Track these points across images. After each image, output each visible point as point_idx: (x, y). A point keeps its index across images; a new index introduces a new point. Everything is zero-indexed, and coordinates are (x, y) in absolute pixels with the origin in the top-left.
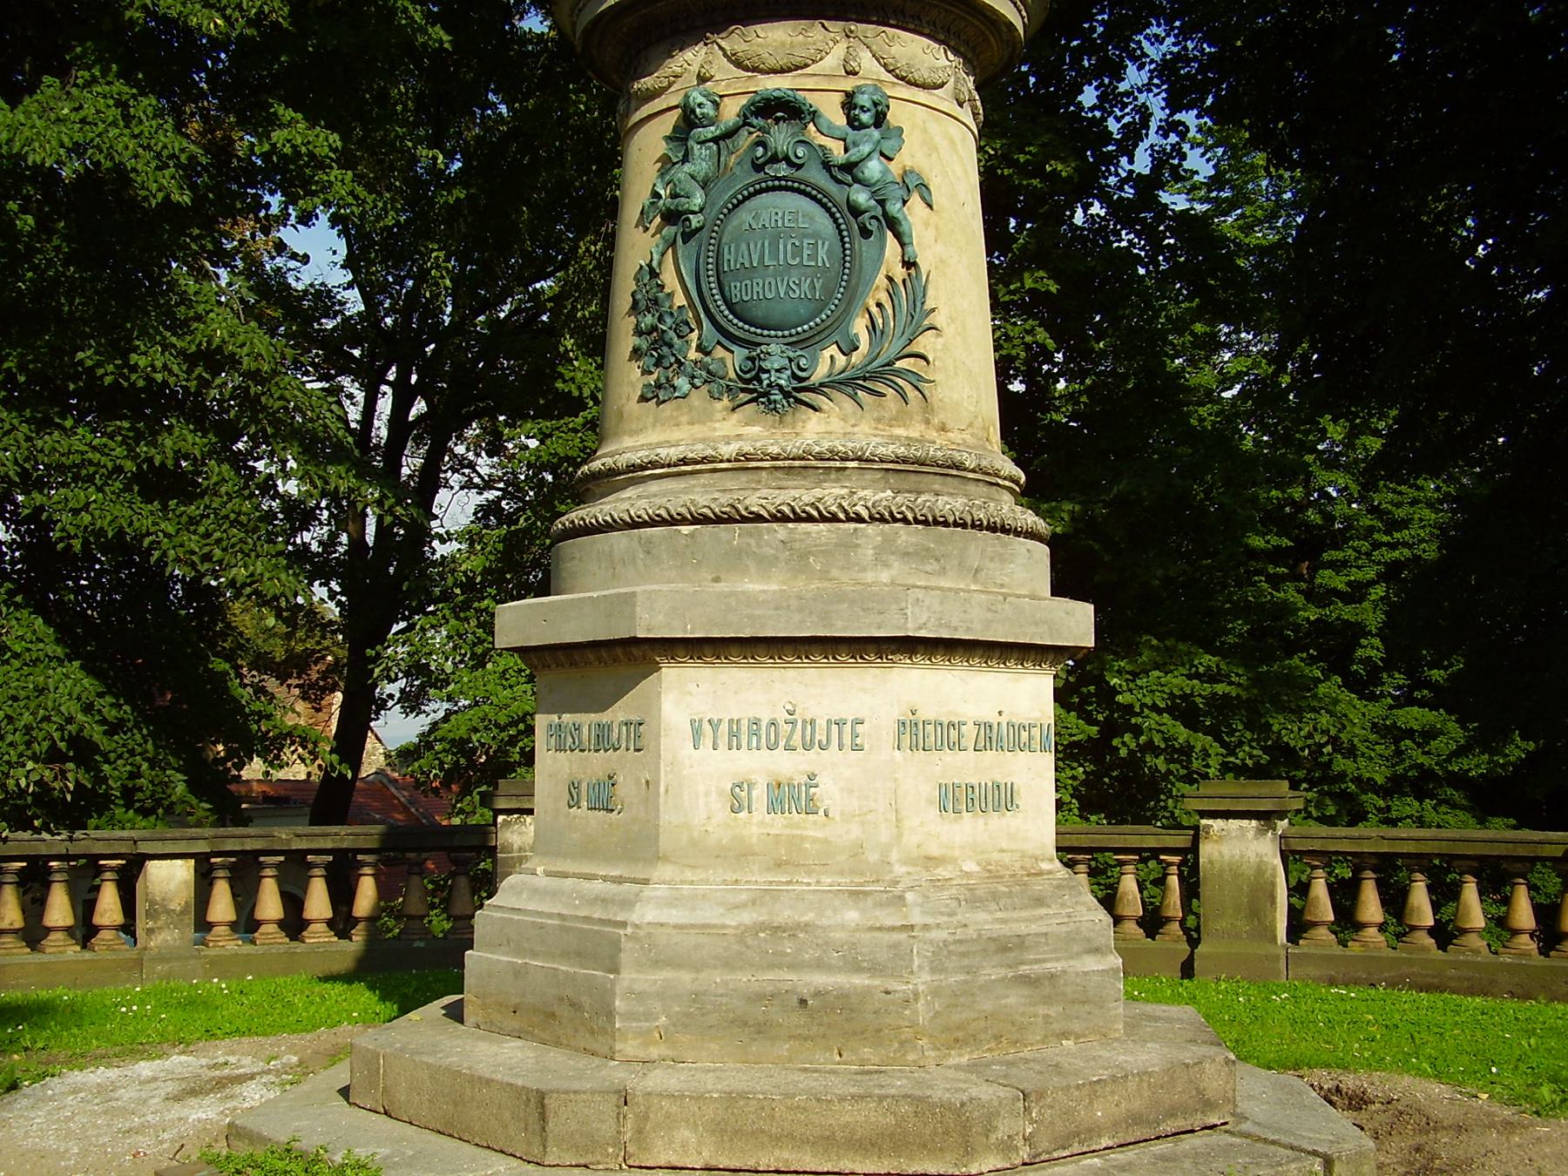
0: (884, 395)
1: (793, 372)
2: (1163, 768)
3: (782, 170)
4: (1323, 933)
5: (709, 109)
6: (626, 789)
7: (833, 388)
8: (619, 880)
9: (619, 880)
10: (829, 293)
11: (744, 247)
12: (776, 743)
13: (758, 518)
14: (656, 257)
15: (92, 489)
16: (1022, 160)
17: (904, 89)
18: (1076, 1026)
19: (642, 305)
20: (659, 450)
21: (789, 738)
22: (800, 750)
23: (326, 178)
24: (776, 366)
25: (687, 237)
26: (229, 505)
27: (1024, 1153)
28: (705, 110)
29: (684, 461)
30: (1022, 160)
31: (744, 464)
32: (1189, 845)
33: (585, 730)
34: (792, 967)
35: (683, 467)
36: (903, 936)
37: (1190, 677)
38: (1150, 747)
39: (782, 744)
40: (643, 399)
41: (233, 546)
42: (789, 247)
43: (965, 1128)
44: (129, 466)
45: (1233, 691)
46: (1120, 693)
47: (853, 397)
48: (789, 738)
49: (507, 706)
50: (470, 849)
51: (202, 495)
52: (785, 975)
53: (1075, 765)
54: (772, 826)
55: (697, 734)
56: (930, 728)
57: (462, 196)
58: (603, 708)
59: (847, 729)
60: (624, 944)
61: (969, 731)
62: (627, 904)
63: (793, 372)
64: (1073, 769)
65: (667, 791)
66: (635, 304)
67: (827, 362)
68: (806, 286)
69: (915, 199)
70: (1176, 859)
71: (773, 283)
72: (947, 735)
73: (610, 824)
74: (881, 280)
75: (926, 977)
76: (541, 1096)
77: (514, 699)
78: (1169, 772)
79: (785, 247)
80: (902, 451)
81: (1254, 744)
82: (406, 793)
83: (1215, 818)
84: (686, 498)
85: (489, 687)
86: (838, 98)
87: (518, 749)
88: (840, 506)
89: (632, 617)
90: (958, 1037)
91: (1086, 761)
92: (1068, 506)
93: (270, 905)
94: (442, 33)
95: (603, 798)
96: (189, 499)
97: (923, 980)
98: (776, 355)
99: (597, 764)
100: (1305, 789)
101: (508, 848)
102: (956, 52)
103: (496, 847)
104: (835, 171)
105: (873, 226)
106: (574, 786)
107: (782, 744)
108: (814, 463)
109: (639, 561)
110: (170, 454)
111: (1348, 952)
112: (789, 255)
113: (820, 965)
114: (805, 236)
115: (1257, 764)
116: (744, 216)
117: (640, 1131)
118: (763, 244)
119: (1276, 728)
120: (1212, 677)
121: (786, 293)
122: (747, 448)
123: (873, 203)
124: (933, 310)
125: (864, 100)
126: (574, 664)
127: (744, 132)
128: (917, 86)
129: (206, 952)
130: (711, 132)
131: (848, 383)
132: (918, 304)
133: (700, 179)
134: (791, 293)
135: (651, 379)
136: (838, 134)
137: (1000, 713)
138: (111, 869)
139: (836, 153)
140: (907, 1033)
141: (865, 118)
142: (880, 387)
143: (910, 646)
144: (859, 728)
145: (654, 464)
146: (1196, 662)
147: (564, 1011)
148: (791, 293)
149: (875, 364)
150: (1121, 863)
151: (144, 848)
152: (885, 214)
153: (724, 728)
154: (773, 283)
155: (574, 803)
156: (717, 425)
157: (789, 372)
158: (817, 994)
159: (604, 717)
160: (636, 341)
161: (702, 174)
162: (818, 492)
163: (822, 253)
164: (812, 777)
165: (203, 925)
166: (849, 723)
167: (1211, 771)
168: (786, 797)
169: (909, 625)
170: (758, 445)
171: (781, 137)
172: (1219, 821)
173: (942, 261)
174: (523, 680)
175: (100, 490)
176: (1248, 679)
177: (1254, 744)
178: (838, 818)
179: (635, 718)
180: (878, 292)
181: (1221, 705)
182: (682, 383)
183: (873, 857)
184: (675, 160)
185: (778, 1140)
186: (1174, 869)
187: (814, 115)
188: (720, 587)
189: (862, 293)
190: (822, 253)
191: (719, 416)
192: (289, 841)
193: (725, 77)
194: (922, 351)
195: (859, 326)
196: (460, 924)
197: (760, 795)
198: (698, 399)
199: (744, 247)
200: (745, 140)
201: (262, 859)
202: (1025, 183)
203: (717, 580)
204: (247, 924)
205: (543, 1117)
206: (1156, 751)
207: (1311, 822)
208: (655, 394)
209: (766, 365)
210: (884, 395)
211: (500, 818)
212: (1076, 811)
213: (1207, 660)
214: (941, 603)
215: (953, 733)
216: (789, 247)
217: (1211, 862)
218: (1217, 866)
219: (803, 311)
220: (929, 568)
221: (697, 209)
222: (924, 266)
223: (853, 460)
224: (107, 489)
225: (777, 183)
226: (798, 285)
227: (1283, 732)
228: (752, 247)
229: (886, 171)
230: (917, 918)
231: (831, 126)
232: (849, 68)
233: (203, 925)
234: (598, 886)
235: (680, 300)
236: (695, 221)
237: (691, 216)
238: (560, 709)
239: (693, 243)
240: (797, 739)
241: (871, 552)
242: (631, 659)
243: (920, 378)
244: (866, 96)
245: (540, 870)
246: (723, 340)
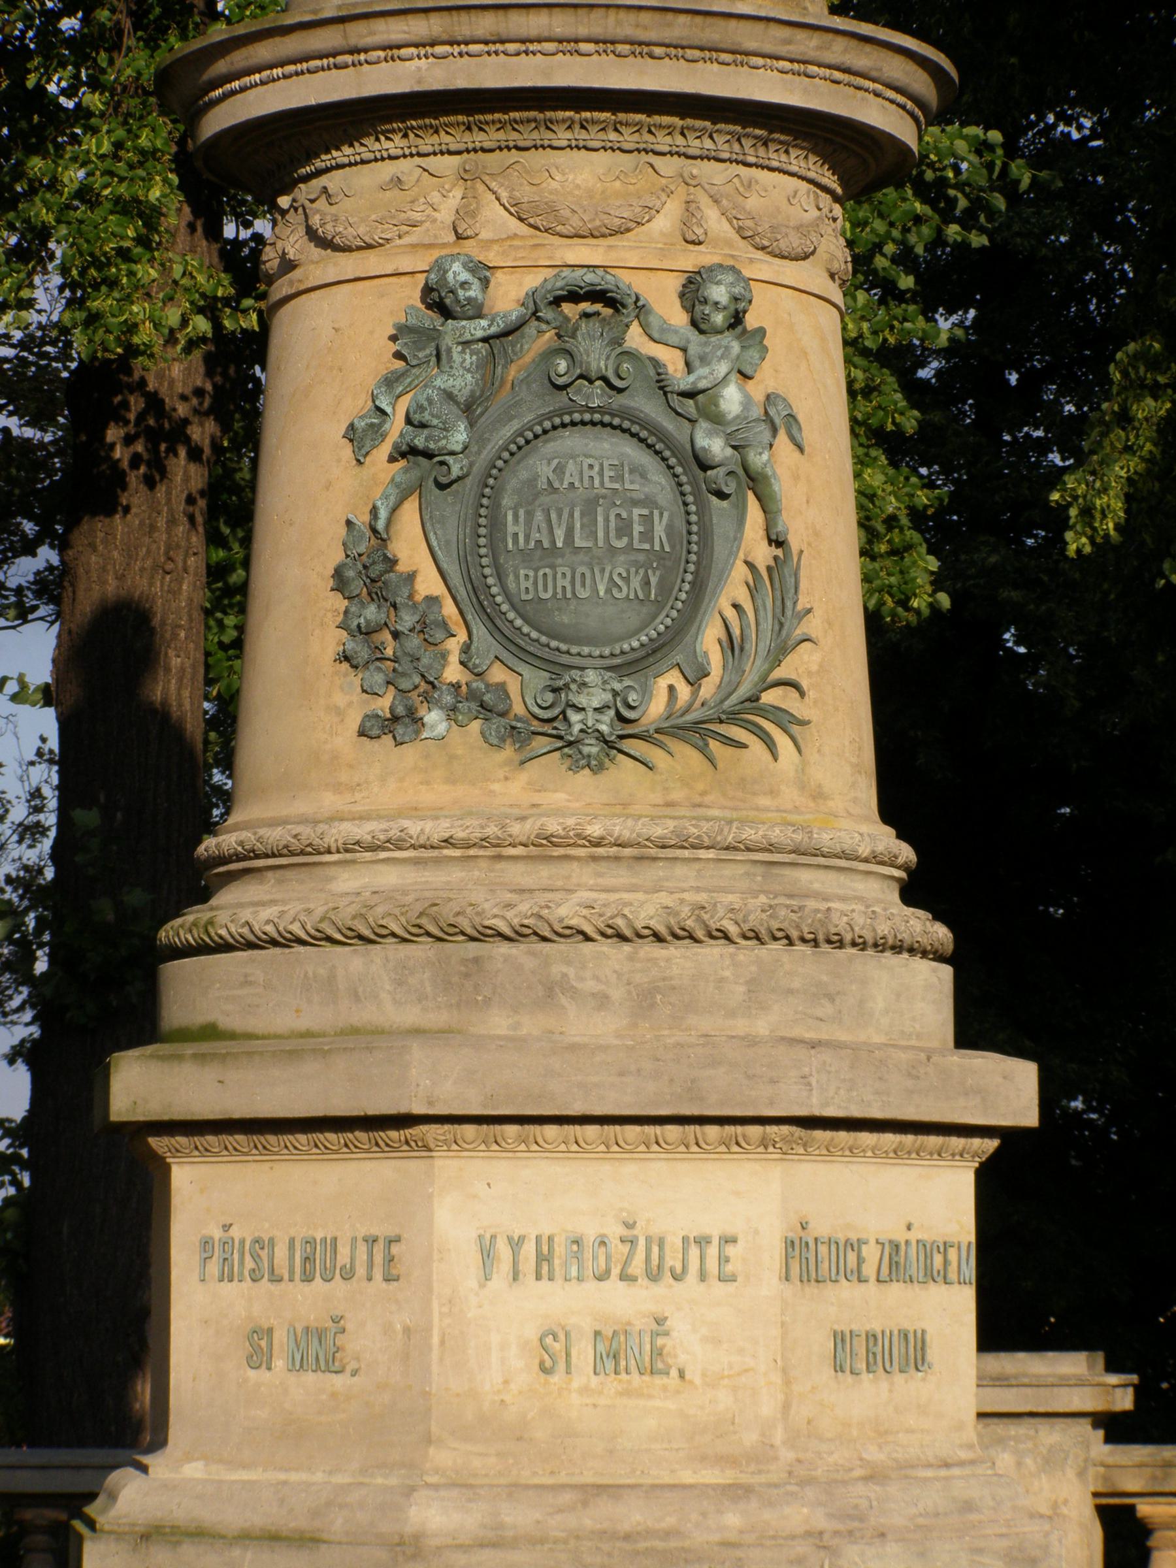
0: (745, 746)
1: (618, 714)
3: (596, 396)
7: (673, 735)
11: (539, 516)
12: (608, 1272)
14: (383, 514)
17: (765, 267)
20: (406, 823)
21: (626, 1263)
22: (643, 1281)
24: (596, 704)
28: (472, 293)
33: (281, 1252)
39: (616, 1271)
42: (612, 518)
47: (703, 750)
48: (626, 1263)
54: (600, 1393)
55: (487, 1253)
56: (823, 1249)
59: (712, 1251)
61: (871, 1253)
63: (618, 714)
65: (442, 1343)
68: (636, 582)
71: (588, 575)
73: (333, 1395)
76: (981, 1415)
79: (607, 520)
86: (674, 283)
88: (699, 919)
104: (675, 401)
107: (616, 1271)
108: (654, 852)
109: (383, 995)
112: (612, 534)
114: (636, 503)
118: (571, 515)
121: (608, 591)
122: (553, 826)
123: (729, 451)
124: (809, 611)
125: (719, 293)
127: (532, 328)
128: (784, 257)
132: (789, 604)
133: (462, 400)
134: (615, 592)
136: (674, 340)
137: (909, 1228)
139: (671, 369)
144: (730, 1250)
148: (615, 592)
149: (727, 703)
153: (529, 1249)
154: (588, 575)
156: (496, 787)
157: (612, 713)
161: (466, 392)
163: (659, 530)
164: (660, 1321)
166: (715, 1242)
169: (814, 1100)
170: (571, 822)
173: (817, 534)
178: (698, 1381)
183: (750, 1438)
184: (414, 362)
187: (641, 309)
189: (714, 593)
190: (659, 530)
191: (501, 774)
194: (793, 676)
195: (710, 639)
197: (584, 1353)
199: (539, 516)
200: (539, 340)
209: (581, 700)
210: (745, 746)
214: (852, 1067)
216: (612, 518)
220: (819, 1012)
221: (458, 448)
222: (795, 543)
223: (708, 848)
225: (587, 417)
226: (627, 580)
228: (554, 516)
231: (666, 328)
235: (429, 584)
237: (450, 459)
240: (637, 1266)
241: (742, 989)
244: (722, 289)
246: (505, 655)
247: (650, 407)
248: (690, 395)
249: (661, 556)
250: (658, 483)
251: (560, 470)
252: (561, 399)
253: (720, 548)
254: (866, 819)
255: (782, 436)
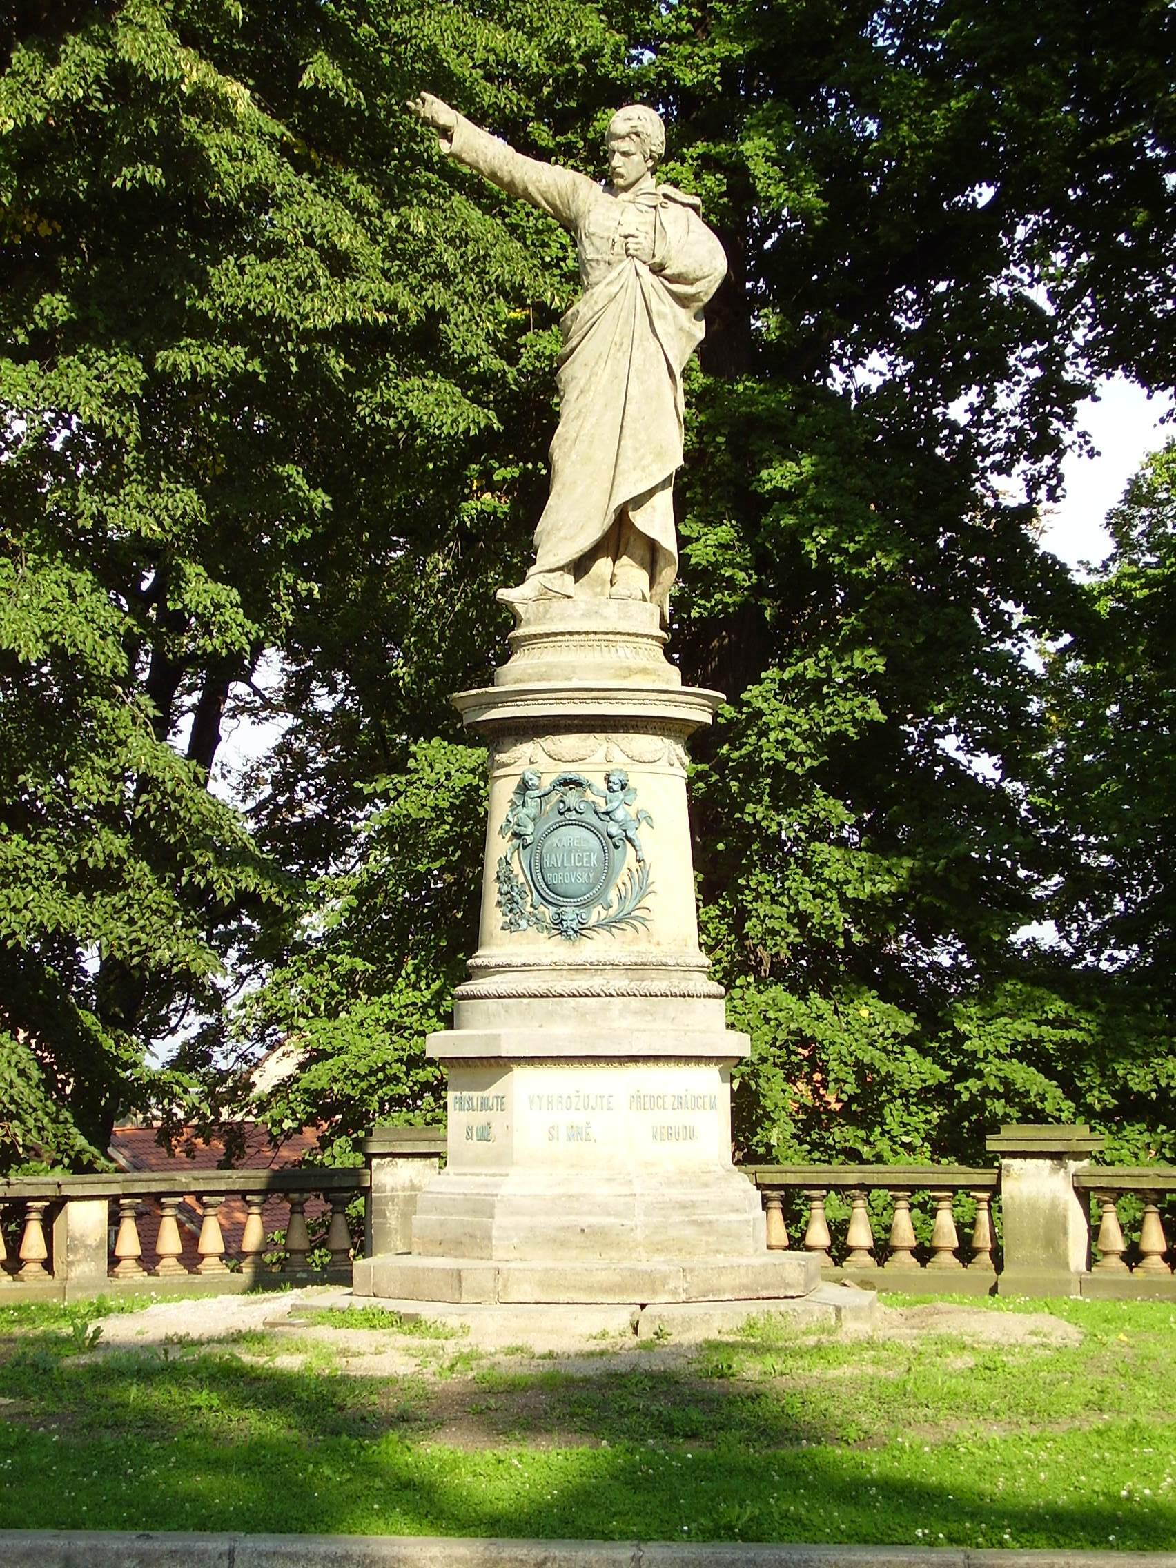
2: (1000, 1112)
3: (573, 815)
4: (1115, 1262)
5: (536, 782)
6: (496, 1130)
8: (494, 1175)
9: (494, 1175)
10: (597, 879)
13: (561, 996)
15: (30, 889)
16: (851, 550)
18: (725, 1248)
19: (502, 879)
23: (222, 619)
25: (525, 847)
26: (150, 896)
27: (683, 1297)
29: (525, 965)
30: (851, 550)
31: (555, 967)
32: (994, 1182)
34: (577, 1214)
35: (525, 967)
36: (630, 1199)
37: (1039, 1023)
38: (985, 1091)
40: (503, 928)
41: (156, 931)
43: (653, 1282)
44: (62, 870)
45: (1080, 1036)
46: (970, 1038)
47: (610, 932)
49: (366, 1055)
50: (347, 1189)
51: (126, 887)
52: (572, 1218)
53: (929, 1109)
56: (647, 1099)
57: (308, 536)
58: (484, 1089)
59: (605, 1100)
60: (497, 1205)
62: (497, 1186)
64: (926, 1113)
66: (498, 878)
67: (596, 914)
68: (585, 877)
69: (644, 823)
70: (985, 1195)
72: (656, 1101)
74: (625, 871)
75: (642, 1218)
76: (459, 1271)
77: (373, 1049)
78: (1007, 1115)
80: (634, 960)
81: (1103, 1089)
82: (126, 1152)
83: (1015, 1158)
84: (525, 985)
85: (347, 1037)
87: (376, 1098)
89: (499, 1046)
90: (660, 1248)
91: (939, 1104)
92: (908, 863)
93: (170, 1240)
94: (323, 495)
95: (485, 1135)
96: (113, 890)
97: (640, 1219)
98: (570, 913)
99: (479, 1118)
100: (1163, 1132)
101: (381, 1189)
102: (669, 737)
103: (370, 1187)
105: (619, 843)
106: (469, 1129)
110: (101, 856)
111: (1133, 1278)
113: (590, 1213)
115: (1104, 1108)
116: (553, 839)
117: (505, 1286)
119: (1120, 1073)
120: (1061, 1023)
126: (469, 1066)
129: (116, 1282)
130: (536, 793)
131: (607, 925)
135: (507, 919)
138: (37, 1210)
140: (632, 1245)
141: (615, 787)
142: (623, 926)
143: (634, 1059)
145: (510, 966)
146: (1047, 1008)
147: (466, 1240)
150: (938, 1199)
151: (66, 1191)
152: (626, 837)
155: (469, 1137)
158: (589, 1226)
159: (485, 1094)
160: (499, 897)
162: (591, 983)
163: (593, 859)
165: (114, 1261)
167: (1064, 1116)
168: (576, 1134)
171: (572, 798)
172: (1018, 1161)
174: (382, 1029)
175: (36, 889)
176: (1098, 1025)
177: (1103, 1089)
179: (501, 1095)
180: (623, 876)
181: (1073, 1052)
182: (523, 923)
185: (568, 1289)
186: (984, 1205)
188: (542, 1030)
190: (593, 859)
192: (188, 1184)
193: (544, 763)
195: (613, 895)
196: (338, 1257)
198: (532, 931)
200: (555, 797)
201: (163, 1200)
202: (854, 571)
203: (541, 1026)
204: (149, 1259)
205: (460, 1281)
206: (996, 1095)
207: (1163, 1163)
208: (510, 926)
211: (375, 1162)
212: (928, 1155)
213: (1057, 1007)
215: (660, 1102)
217: (1012, 1198)
218: (1017, 1201)
219: (584, 889)
224: (42, 888)
227: (1129, 1077)
229: (627, 814)
230: (638, 1190)
232: (610, 758)
233: (114, 1261)
234: (482, 1179)
235: (522, 879)
236: (529, 839)
238: (462, 1089)
239: (528, 849)
240: (580, 1106)
242: (499, 1065)
243: (645, 919)
245: (451, 1173)
247: (591, 818)
248: (607, 813)
249: (595, 868)
250: (594, 842)
251: (560, 840)
252: (562, 818)
253: (617, 863)
254: (658, 660)
255: (644, 823)
